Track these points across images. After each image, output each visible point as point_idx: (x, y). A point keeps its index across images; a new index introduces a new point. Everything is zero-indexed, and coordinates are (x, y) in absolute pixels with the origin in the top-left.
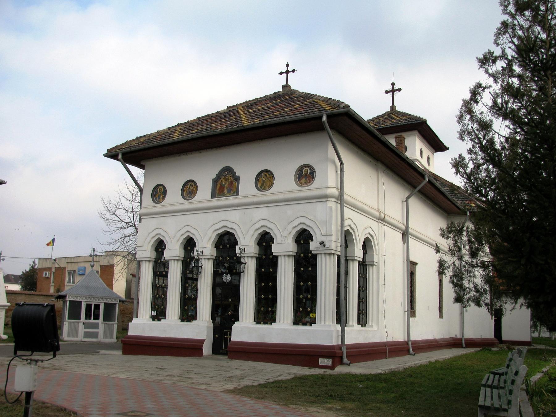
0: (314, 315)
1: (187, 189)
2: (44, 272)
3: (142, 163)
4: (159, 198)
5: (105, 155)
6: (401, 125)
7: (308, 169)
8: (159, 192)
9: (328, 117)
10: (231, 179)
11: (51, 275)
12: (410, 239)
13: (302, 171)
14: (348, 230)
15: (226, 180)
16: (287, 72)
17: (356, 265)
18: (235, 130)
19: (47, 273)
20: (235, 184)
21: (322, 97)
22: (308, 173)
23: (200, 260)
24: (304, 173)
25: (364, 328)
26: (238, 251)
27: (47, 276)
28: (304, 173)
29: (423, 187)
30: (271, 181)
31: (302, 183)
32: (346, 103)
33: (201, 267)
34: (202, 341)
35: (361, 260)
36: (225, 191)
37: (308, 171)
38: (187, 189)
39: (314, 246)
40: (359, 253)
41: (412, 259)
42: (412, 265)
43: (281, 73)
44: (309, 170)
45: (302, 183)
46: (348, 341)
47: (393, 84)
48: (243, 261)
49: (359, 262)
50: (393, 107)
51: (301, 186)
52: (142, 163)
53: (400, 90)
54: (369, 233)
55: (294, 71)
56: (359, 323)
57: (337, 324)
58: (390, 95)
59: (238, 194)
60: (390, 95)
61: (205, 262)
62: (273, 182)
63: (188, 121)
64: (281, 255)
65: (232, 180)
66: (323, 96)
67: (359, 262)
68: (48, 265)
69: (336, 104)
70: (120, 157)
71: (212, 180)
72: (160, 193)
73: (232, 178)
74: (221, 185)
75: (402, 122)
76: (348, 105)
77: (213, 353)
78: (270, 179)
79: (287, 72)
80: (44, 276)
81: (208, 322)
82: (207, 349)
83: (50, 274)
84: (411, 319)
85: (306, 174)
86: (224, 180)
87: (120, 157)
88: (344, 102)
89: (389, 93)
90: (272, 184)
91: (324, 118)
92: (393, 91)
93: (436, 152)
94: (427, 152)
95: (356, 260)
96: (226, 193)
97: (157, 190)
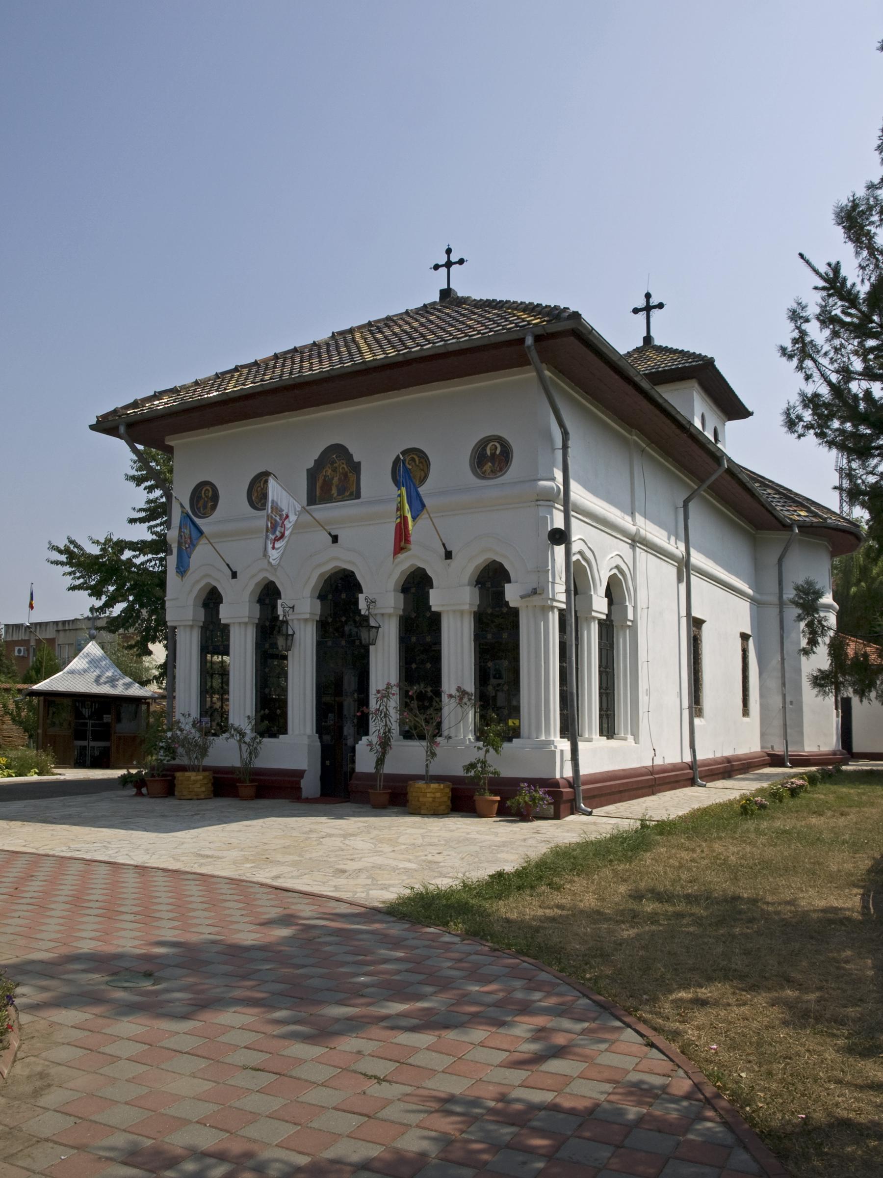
0: (517, 722)
1: (259, 489)
2: (17, 649)
3: (170, 441)
4: (205, 507)
5: (92, 427)
6: (665, 370)
7: (496, 444)
8: (203, 496)
9: (538, 338)
10: (343, 468)
11: (29, 654)
12: (692, 576)
13: (484, 449)
14: (578, 560)
15: (334, 470)
16: (449, 264)
17: (595, 628)
18: (349, 370)
19: (22, 648)
20: (352, 477)
21: (522, 303)
22: (498, 452)
23: (290, 623)
24: (489, 453)
25: (612, 743)
26: (362, 605)
27: (22, 654)
28: (489, 453)
29: (716, 479)
30: (423, 470)
31: (485, 471)
32: (573, 309)
33: (293, 635)
34: (300, 774)
35: (604, 617)
36: (334, 491)
37: (496, 448)
38: (259, 489)
39: (512, 594)
40: (600, 605)
41: (695, 613)
42: (696, 623)
43: (436, 267)
44: (498, 446)
45: (485, 471)
46: (585, 770)
47: (648, 296)
48: (372, 623)
49: (601, 623)
50: (648, 339)
51: (484, 478)
52: (170, 441)
53: (661, 306)
54: (617, 567)
55: (461, 262)
56: (601, 734)
57: (561, 737)
58: (642, 316)
59: (358, 496)
60: (642, 316)
61: (191, 634)
62: (428, 471)
63: (256, 361)
64: (448, 611)
65: (346, 469)
66: (523, 301)
67: (601, 623)
68: (21, 636)
69: (554, 314)
70: (122, 429)
71: (308, 470)
72: (206, 499)
73: (345, 467)
74: (324, 480)
75: (666, 364)
76: (577, 312)
77: (530, 364)
78: (421, 465)
79: (449, 264)
80: (16, 654)
81: (309, 737)
82: (311, 785)
83: (28, 650)
84: (697, 721)
85: (493, 454)
86: (330, 471)
87: (122, 429)
88: (568, 309)
89: (641, 313)
90: (426, 476)
91: (529, 341)
92: (648, 308)
93: (729, 420)
94: (713, 421)
95: (594, 618)
96: (335, 495)
97: (200, 493)
